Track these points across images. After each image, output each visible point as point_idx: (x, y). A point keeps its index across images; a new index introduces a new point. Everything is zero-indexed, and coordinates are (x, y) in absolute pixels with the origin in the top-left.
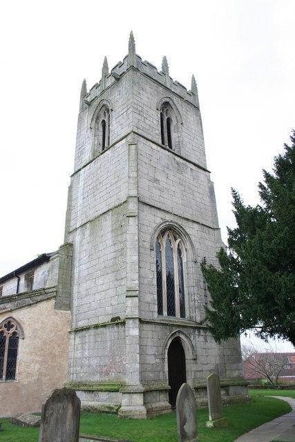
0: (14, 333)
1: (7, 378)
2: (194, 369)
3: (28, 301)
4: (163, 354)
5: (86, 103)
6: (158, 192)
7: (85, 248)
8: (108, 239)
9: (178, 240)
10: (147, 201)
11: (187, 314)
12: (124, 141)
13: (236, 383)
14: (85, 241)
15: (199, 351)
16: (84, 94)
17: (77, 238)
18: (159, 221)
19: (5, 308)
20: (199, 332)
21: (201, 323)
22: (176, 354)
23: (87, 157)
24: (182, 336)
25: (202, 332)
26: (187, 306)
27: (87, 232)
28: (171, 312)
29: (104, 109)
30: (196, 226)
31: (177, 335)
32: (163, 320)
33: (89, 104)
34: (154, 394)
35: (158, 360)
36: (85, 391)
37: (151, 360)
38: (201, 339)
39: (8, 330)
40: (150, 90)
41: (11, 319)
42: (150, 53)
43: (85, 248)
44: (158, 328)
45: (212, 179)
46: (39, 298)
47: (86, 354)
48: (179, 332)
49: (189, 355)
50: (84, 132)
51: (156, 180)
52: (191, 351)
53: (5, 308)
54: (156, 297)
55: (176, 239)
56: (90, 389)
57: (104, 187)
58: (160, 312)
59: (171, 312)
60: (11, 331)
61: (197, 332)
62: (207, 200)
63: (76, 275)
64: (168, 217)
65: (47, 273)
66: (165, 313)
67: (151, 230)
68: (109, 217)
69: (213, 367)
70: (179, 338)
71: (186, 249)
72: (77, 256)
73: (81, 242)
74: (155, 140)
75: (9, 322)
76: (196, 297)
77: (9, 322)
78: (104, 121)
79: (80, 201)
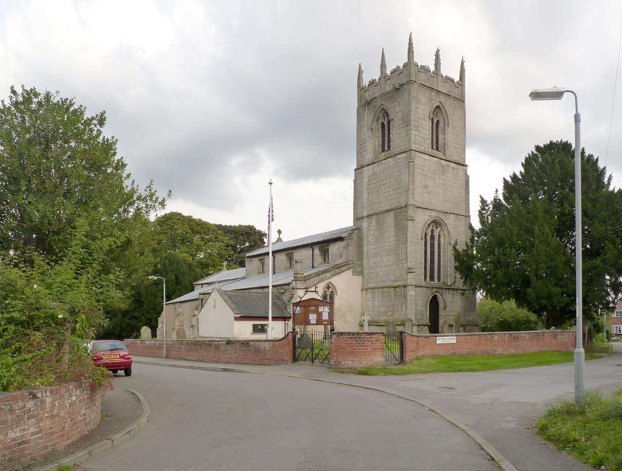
0: (332, 292)
1: (235, 317)
2: (445, 314)
3: (338, 271)
4: (426, 305)
5: (365, 104)
6: (427, 196)
7: (371, 233)
8: (392, 231)
9: (439, 229)
10: (420, 205)
11: (442, 280)
12: (404, 155)
13: (471, 324)
14: (371, 228)
15: (448, 304)
16: (361, 89)
17: (365, 224)
18: (427, 218)
19: (326, 277)
20: (449, 291)
21: (450, 286)
22: (434, 304)
23: (369, 156)
24: (438, 294)
25: (451, 291)
26: (442, 274)
27: (374, 222)
28: (432, 278)
29: (383, 112)
30: (452, 215)
31: (435, 293)
32: (427, 285)
33: (368, 103)
34: (421, 326)
35: (424, 309)
36: (379, 325)
37: (420, 308)
38: (450, 295)
39: (328, 290)
40: (425, 99)
41: (329, 284)
42: (424, 58)
43: (371, 233)
44: (425, 289)
45: (468, 174)
46: (344, 268)
47: (376, 303)
48: (436, 291)
49: (441, 306)
50: (365, 129)
51: (426, 186)
52: (443, 303)
53: (326, 277)
54: (423, 270)
55: (437, 228)
56: (379, 324)
57: (387, 190)
58: (425, 279)
59: (432, 278)
60: (331, 290)
61: (447, 292)
62: (463, 191)
63: (365, 252)
64: (434, 214)
65: (342, 249)
66: (428, 279)
67: (422, 226)
68: (392, 214)
69: (456, 313)
70: (436, 295)
71: (444, 235)
72: (365, 237)
73: (368, 228)
74: (422, 149)
75: (328, 285)
76: (449, 269)
77: (328, 285)
78: (383, 124)
79: (365, 196)
